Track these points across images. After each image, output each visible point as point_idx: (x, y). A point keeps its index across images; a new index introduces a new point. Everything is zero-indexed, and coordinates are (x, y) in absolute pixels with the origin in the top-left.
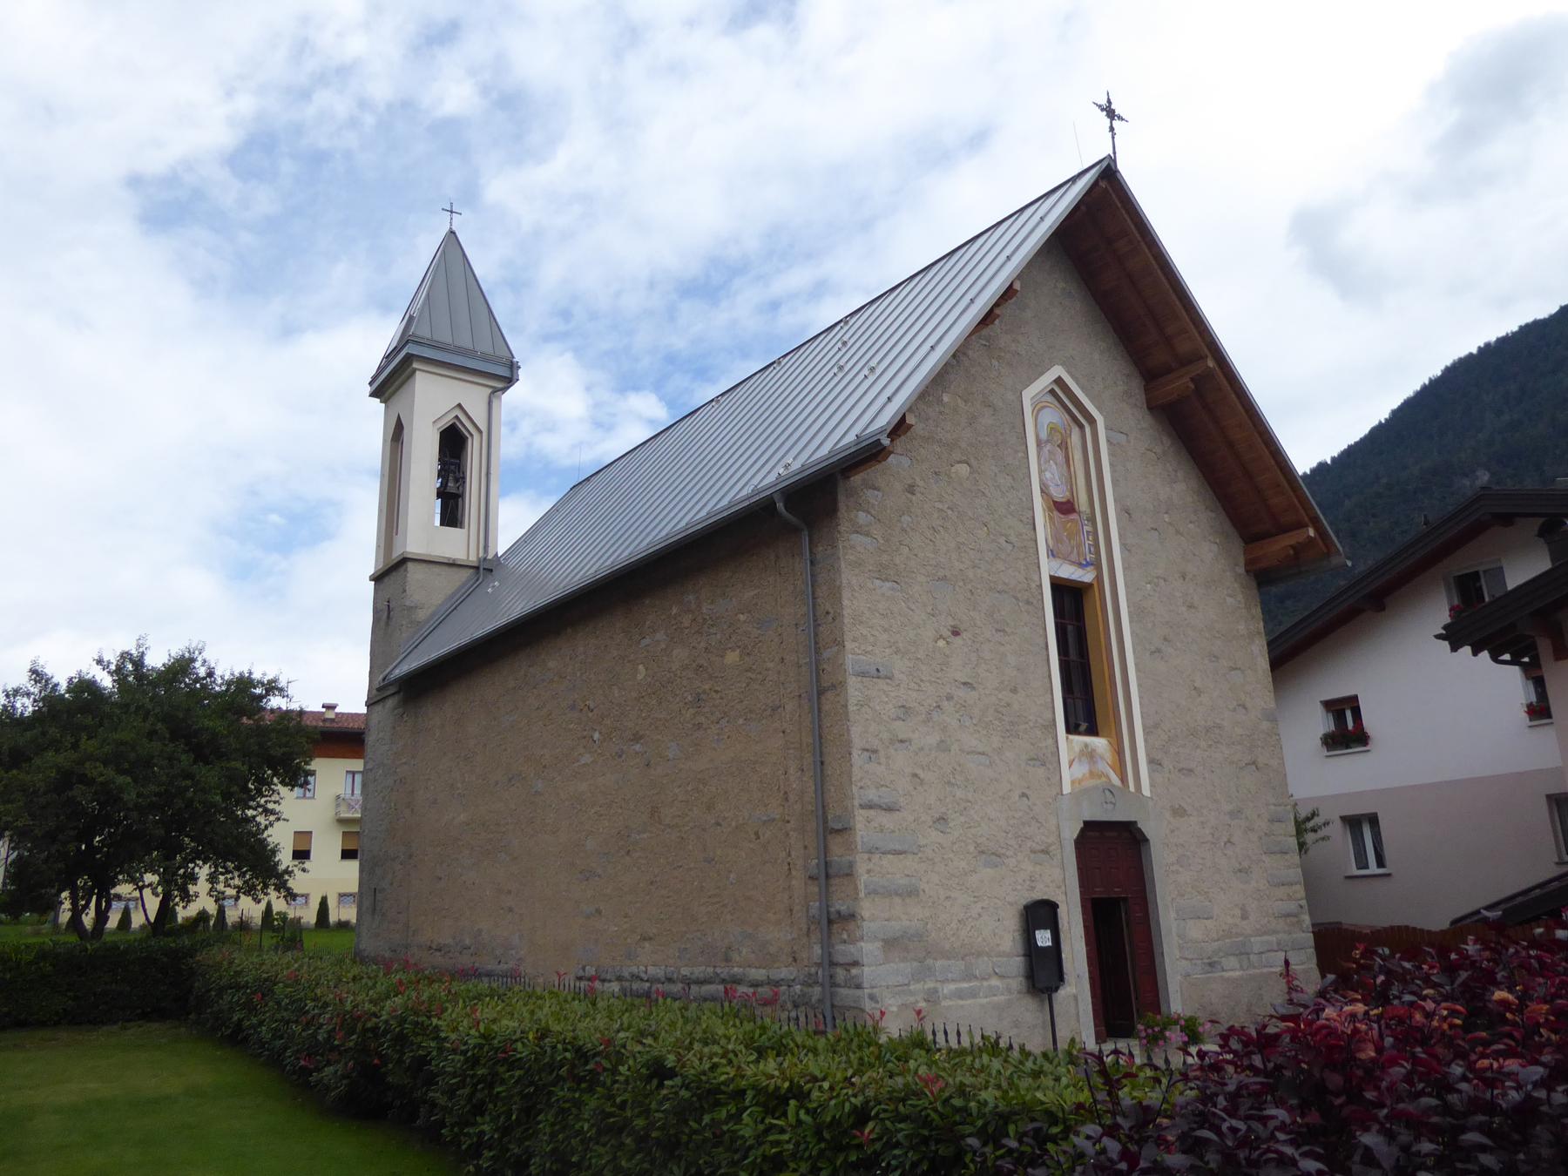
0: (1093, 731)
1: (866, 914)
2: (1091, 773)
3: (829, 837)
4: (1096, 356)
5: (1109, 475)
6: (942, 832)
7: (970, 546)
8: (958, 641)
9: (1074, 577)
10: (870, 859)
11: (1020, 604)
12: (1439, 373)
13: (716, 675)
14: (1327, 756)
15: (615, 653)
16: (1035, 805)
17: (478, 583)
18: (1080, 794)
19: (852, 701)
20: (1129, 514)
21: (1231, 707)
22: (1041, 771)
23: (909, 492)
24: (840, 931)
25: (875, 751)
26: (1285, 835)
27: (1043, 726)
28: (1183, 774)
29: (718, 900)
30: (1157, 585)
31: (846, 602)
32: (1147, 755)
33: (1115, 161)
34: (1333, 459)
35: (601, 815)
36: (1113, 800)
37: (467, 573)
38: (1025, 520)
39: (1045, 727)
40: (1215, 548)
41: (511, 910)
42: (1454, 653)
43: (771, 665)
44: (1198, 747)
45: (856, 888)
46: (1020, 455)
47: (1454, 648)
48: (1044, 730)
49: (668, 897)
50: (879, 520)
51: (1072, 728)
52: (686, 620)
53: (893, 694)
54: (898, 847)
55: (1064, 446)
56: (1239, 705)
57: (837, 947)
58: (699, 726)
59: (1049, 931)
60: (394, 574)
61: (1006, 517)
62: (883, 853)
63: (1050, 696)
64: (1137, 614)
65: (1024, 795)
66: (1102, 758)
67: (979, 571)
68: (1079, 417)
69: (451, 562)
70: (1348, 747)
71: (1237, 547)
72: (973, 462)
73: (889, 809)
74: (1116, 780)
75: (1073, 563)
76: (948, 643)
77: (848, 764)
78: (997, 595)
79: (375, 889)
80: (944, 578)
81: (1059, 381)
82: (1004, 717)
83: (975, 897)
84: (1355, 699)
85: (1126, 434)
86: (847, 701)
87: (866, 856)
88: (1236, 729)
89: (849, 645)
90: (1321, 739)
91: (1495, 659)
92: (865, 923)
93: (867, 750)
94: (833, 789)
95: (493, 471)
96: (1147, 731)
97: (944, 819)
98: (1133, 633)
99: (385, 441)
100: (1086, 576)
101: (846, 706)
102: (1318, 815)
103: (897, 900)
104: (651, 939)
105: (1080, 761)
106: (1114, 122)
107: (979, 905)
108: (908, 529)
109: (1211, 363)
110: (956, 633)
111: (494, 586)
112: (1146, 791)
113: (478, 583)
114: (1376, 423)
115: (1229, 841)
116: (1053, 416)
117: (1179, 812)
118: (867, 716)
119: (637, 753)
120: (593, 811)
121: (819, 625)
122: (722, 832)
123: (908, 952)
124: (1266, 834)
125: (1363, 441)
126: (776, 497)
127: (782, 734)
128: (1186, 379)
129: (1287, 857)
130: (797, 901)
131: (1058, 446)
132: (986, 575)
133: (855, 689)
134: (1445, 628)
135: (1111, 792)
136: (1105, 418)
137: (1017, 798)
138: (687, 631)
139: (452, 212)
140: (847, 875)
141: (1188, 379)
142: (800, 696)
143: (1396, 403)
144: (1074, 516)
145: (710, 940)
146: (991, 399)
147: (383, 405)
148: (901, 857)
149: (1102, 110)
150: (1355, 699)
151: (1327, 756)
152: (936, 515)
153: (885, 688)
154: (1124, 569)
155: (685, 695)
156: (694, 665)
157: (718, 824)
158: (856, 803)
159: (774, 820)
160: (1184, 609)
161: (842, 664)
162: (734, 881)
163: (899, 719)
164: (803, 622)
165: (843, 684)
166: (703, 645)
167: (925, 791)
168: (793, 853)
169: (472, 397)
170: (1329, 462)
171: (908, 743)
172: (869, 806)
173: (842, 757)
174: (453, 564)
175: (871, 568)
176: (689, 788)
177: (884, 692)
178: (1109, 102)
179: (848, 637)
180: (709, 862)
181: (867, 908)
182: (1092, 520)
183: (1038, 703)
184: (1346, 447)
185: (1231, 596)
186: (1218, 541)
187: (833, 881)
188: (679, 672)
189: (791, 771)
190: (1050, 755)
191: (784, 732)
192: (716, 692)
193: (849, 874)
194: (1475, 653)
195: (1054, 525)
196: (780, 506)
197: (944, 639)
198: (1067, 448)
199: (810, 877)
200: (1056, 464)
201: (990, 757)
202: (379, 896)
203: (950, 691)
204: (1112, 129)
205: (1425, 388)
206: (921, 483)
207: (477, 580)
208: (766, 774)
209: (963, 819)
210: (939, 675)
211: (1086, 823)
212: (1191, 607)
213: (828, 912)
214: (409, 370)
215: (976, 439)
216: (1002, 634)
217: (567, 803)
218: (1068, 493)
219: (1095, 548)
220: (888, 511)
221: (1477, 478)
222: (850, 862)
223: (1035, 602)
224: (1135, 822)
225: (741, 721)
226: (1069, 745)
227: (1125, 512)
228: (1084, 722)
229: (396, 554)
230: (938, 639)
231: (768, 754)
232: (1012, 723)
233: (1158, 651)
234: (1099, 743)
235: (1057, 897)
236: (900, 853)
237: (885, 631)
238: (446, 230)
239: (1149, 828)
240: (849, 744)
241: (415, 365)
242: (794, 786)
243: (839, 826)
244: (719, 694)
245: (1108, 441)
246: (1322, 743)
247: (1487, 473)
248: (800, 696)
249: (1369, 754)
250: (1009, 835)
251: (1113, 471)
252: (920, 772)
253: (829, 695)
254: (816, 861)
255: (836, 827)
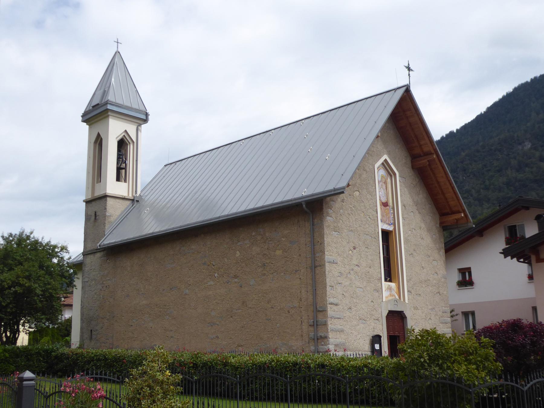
0: (390, 281)
1: (330, 336)
2: (390, 294)
3: (317, 312)
4: (397, 150)
5: (399, 193)
6: (350, 312)
7: (359, 220)
8: (355, 251)
9: (387, 229)
10: (331, 320)
11: (373, 239)
12: (512, 91)
13: (272, 258)
14: (458, 289)
15: (226, 246)
16: (375, 305)
17: (133, 207)
18: (388, 302)
19: (327, 271)
20: (405, 207)
21: (433, 273)
22: (377, 294)
23: (342, 202)
24: (321, 342)
25: (333, 287)
26: (447, 317)
27: (378, 279)
28: (418, 296)
29: (272, 332)
30: (412, 231)
31: (325, 239)
32: (407, 289)
33: (410, 86)
34: (457, 130)
35: (218, 303)
36: (397, 304)
37: (128, 203)
38: (374, 210)
39: (378, 279)
40: (430, 218)
41: (172, 337)
42: (505, 259)
43: (295, 257)
44: (422, 287)
45: (327, 328)
46: (374, 187)
47: (505, 257)
48: (378, 281)
49: (250, 332)
50: (334, 212)
51: (386, 280)
52: (259, 238)
53: (337, 269)
54: (338, 317)
55: (385, 183)
56: (435, 273)
57: (320, 347)
58: (264, 274)
59: (378, 345)
60: (98, 200)
61: (369, 209)
62: (335, 318)
63: (380, 269)
64: (406, 241)
65: (372, 301)
66: (394, 290)
67: (361, 228)
68: (390, 173)
69: (123, 197)
70: (466, 286)
71: (438, 216)
72: (360, 191)
73: (336, 305)
74: (397, 297)
75: (387, 224)
76: (352, 252)
77: (325, 291)
78: (366, 236)
79: (91, 330)
80: (352, 231)
81: (386, 160)
82: (367, 276)
83: (358, 333)
84: (470, 268)
85: (405, 178)
86: (325, 270)
87: (330, 319)
88: (434, 281)
89: (326, 253)
90: (457, 283)
91: (518, 261)
92: (330, 339)
93: (331, 286)
94: (319, 298)
95: (139, 159)
96: (407, 282)
97: (350, 308)
98: (405, 248)
99: (89, 142)
100: (391, 228)
101: (325, 272)
102: (454, 311)
103: (338, 333)
104: (242, 346)
105: (387, 290)
106: (410, 72)
107: (359, 335)
108: (342, 214)
109: (435, 156)
110: (354, 248)
111: (147, 210)
112: (407, 301)
113: (133, 207)
114: (479, 113)
115: (430, 319)
116: (382, 172)
117: (416, 308)
118: (331, 276)
119: (236, 282)
120: (214, 302)
121: (315, 245)
122: (274, 310)
123: (341, 349)
124: (441, 316)
125: (472, 122)
126: (303, 203)
127: (299, 279)
128: (426, 161)
129: (447, 324)
130: (305, 333)
131: (384, 183)
132: (363, 229)
133: (328, 267)
134: (503, 250)
135: (397, 301)
136: (399, 173)
137: (370, 302)
138: (259, 241)
139: (118, 42)
140: (324, 325)
141: (427, 161)
142: (307, 268)
143: (490, 103)
144: (388, 207)
145: (268, 346)
146: (365, 168)
147: (88, 126)
148: (339, 320)
149: (407, 68)
150: (470, 268)
151: (458, 289)
152: (349, 209)
153: (335, 266)
154: (403, 226)
155: (258, 263)
156: (262, 254)
157: (272, 308)
158: (328, 302)
159: (295, 307)
160: (420, 239)
161: (323, 259)
162: (279, 327)
163: (339, 276)
164: (308, 244)
165: (324, 265)
166: (266, 247)
167: (346, 299)
168: (303, 318)
169: (131, 129)
170: (455, 131)
171: (341, 284)
172: (331, 304)
173: (323, 288)
174: (124, 199)
175: (332, 228)
176: (260, 295)
177: (335, 268)
178: (409, 65)
179: (326, 250)
180: (268, 320)
181: (331, 335)
182: (393, 208)
183: (377, 271)
184: (464, 124)
185: (434, 235)
186: (431, 215)
187: (318, 327)
188: (255, 255)
189: (303, 291)
190: (380, 289)
191: (300, 279)
192: (272, 263)
193: (325, 324)
194: (512, 259)
195: (382, 211)
196: (304, 206)
197: (351, 251)
198: (386, 183)
199: (310, 325)
200: (383, 189)
201: (363, 289)
202: (93, 333)
203: (352, 268)
204: (409, 75)
205: (504, 97)
206: (346, 199)
207: (133, 205)
208: (292, 292)
209: (355, 308)
210: (350, 262)
211: (389, 311)
212: (422, 239)
213: (317, 336)
214: (106, 115)
215: (361, 183)
216: (367, 249)
217: (201, 299)
218: (386, 199)
219: (394, 219)
220: (337, 209)
221: (525, 146)
222: (325, 321)
223: (377, 238)
224: (403, 311)
225: (282, 274)
226: (385, 284)
227: (404, 206)
228: (388, 278)
229: (98, 194)
230: (350, 251)
231: (294, 285)
232: (369, 278)
233: (412, 254)
234: (393, 285)
235: (381, 335)
236: (339, 318)
237: (336, 248)
238: (115, 50)
239: (408, 314)
240: (326, 284)
241: (109, 113)
242: (304, 296)
243: (322, 310)
244: (273, 264)
245: (399, 181)
246: (457, 284)
247: (530, 143)
248: (307, 268)
249: (473, 289)
250: (368, 314)
251: (401, 192)
252: (344, 293)
253: (318, 268)
254: (313, 320)
255: (320, 310)
